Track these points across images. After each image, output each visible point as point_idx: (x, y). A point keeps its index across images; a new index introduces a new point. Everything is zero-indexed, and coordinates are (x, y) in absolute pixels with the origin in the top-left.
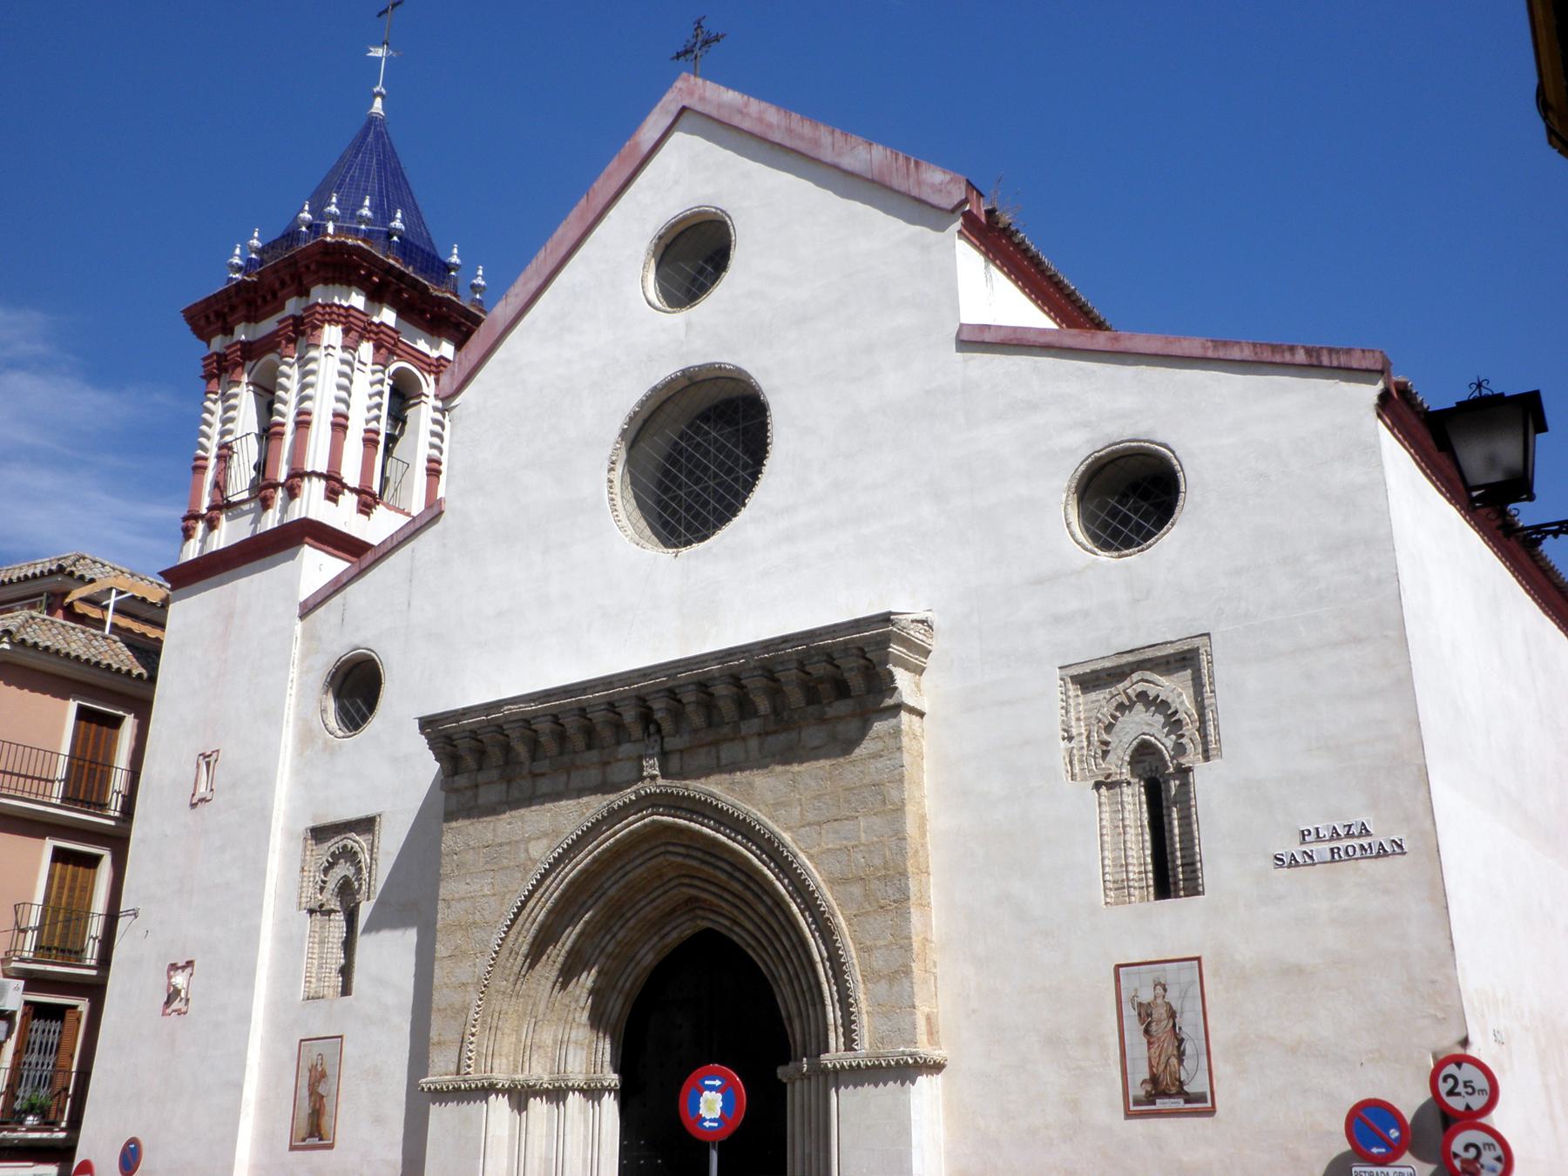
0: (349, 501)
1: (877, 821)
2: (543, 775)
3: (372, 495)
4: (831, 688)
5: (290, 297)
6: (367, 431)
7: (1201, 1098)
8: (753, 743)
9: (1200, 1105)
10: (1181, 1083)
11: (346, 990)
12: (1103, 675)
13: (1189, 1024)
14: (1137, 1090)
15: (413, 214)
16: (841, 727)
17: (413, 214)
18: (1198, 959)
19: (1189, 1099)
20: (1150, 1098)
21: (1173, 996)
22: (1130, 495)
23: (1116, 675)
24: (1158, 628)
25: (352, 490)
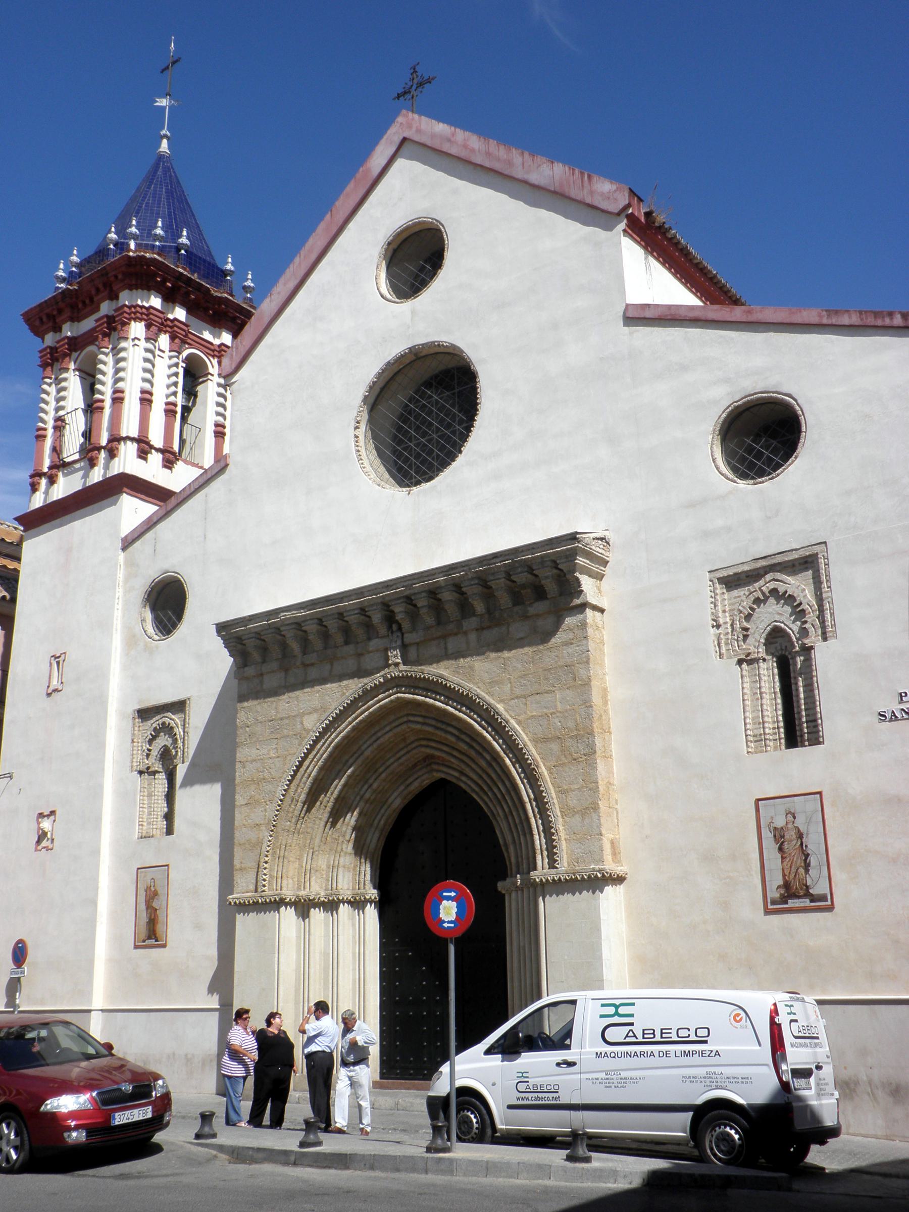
0: (155, 458)
2: (312, 664)
3: (173, 453)
4: (530, 591)
7: (823, 898)
8: (473, 637)
10: (808, 887)
13: (813, 843)
14: (773, 894)
16: (540, 622)
18: (820, 793)
20: (784, 899)
21: (800, 822)
22: (763, 435)
24: (786, 539)
25: (158, 450)
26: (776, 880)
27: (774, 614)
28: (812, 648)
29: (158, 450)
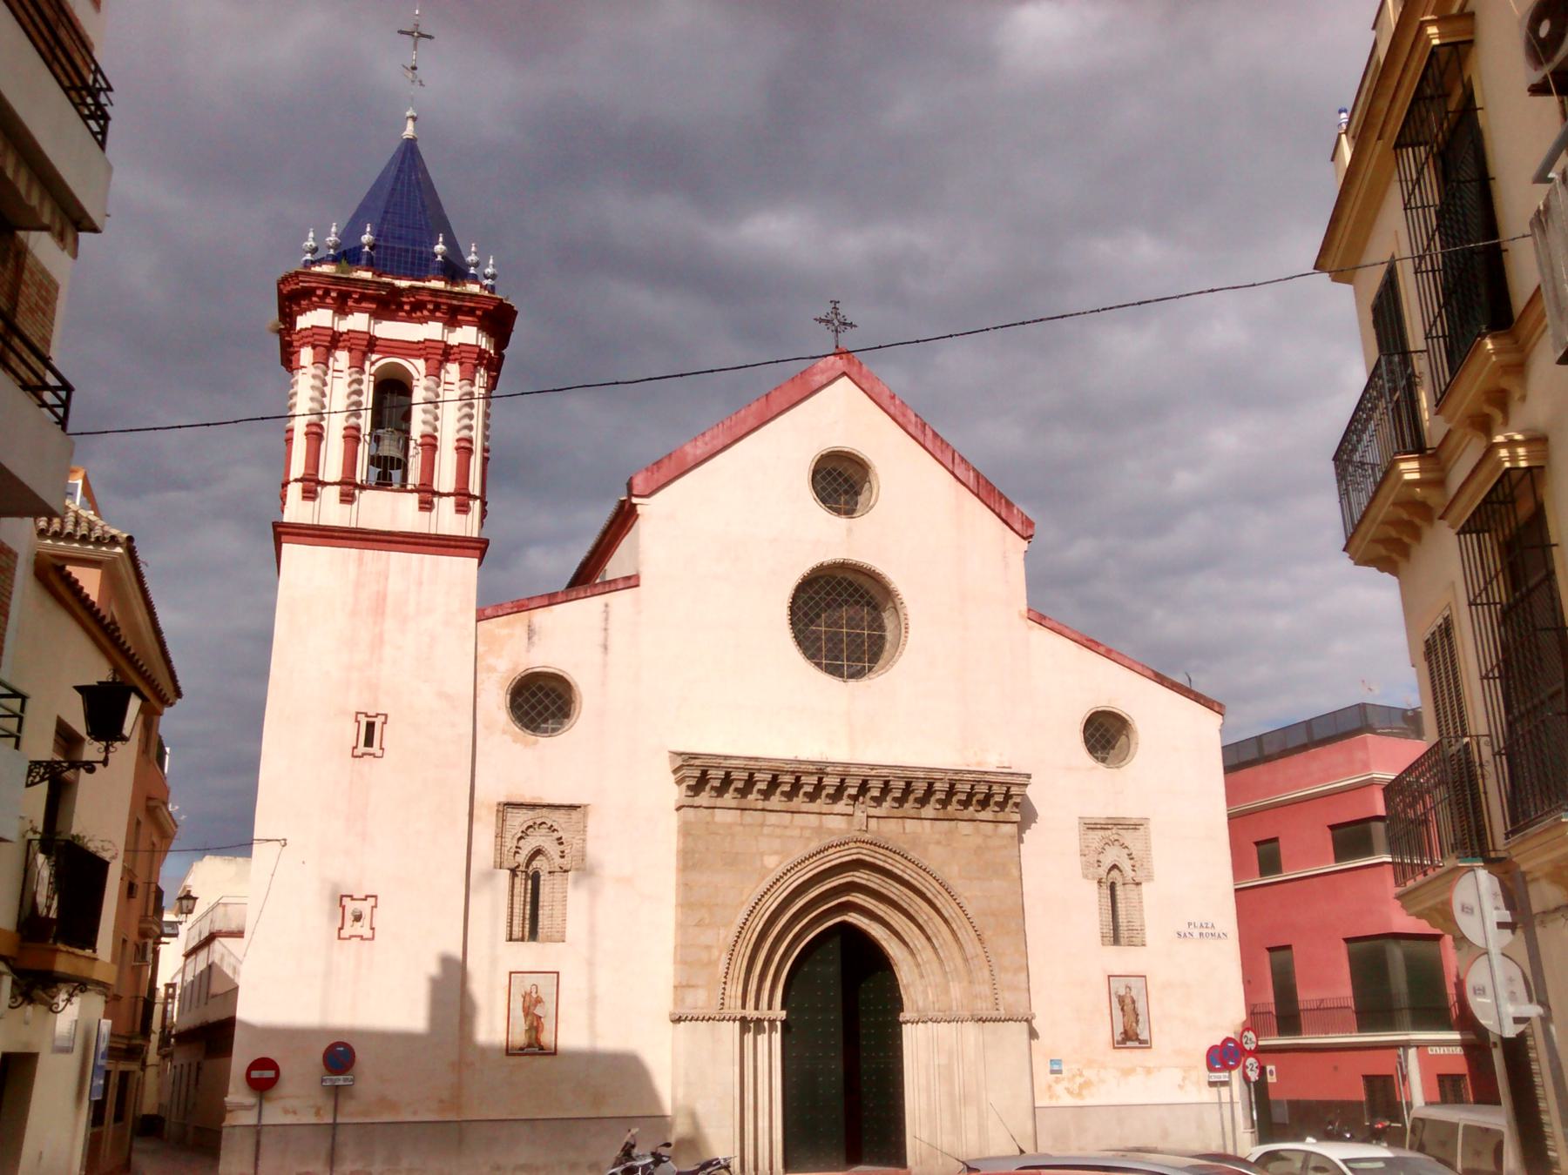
5: (468, 323)
6: (459, 440)
7: (1145, 1042)
9: (1145, 1044)
14: (1118, 1037)
15: (451, 242)
17: (451, 242)
19: (1141, 1042)
21: (1134, 993)
23: (1103, 827)
26: (1119, 1029)
28: (1513, 932)
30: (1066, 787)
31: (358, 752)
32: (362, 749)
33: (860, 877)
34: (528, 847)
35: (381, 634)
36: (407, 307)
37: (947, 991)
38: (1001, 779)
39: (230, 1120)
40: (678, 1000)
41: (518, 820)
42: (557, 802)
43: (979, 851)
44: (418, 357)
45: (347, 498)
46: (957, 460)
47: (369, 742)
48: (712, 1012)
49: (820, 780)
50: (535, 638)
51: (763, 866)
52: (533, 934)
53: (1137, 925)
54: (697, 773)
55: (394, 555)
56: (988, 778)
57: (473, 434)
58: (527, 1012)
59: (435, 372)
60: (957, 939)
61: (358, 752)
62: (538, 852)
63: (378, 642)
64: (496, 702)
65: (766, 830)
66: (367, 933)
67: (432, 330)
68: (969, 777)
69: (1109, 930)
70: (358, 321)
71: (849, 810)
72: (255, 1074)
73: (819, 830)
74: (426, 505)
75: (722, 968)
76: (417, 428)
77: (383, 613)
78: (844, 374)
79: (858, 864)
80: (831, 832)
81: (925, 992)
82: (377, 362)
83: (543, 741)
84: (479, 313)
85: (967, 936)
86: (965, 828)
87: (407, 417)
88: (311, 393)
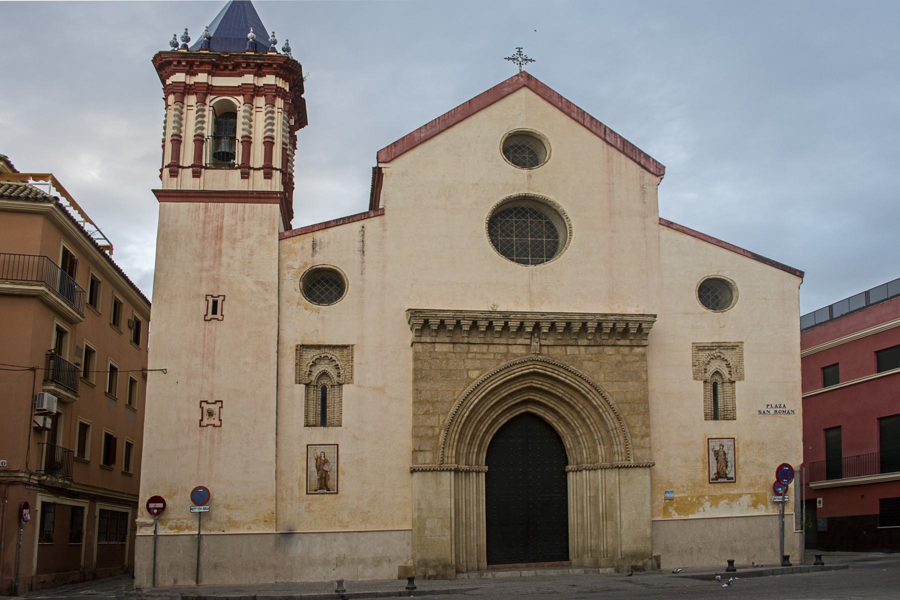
1: (637, 384)
7: (732, 478)
11: (800, 274)
12: (95, 410)
13: (730, 457)
14: (712, 476)
19: (728, 479)
20: (717, 479)
24: (730, 338)
25: (277, 169)
26: (714, 471)
27: (715, 365)
29: (277, 169)
30: (683, 325)
31: (208, 318)
32: (210, 316)
33: (537, 383)
34: (317, 371)
35: (220, 250)
36: (230, 68)
37: (595, 451)
38: (635, 318)
39: (140, 532)
40: (415, 459)
41: (310, 355)
42: (334, 343)
43: (618, 364)
44: (239, 95)
45: (197, 175)
46: (608, 132)
47: (214, 312)
48: (436, 466)
49: (506, 323)
50: (317, 249)
51: (468, 377)
52: (324, 423)
53: (730, 408)
54: (422, 322)
55: (227, 205)
56: (625, 318)
57: (275, 134)
58: (318, 468)
59: (249, 102)
60: (602, 419)
61: (208, 318)
62: (324, 374)
63: (218, 254)
64: (293, 287)
65: (470, 356)
66: (217, 423)
67: (249, 79)
68: (612, 318)
69: (710, 411)
70: (202, 78)
71: (528, 342)
72: (151, 505)
73: (506, 355)
74: (245, 176)
75: (441, 439)
76: (239, 134)
77: (221, 238)
78: (525, 86)
79: (534, 374)
80: (516, 356)
81: (581, 453)
82: (212, 100)
83: (323, 308)
84: (275, 66)
85: (609, 417)
86: (609, 351)
87: (234, 130)
88: (173, 119)
